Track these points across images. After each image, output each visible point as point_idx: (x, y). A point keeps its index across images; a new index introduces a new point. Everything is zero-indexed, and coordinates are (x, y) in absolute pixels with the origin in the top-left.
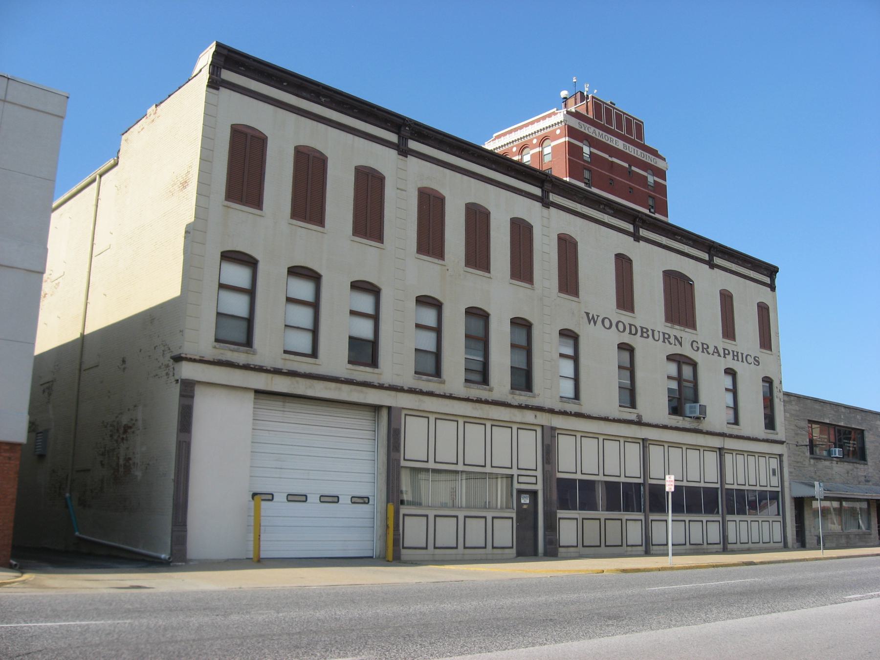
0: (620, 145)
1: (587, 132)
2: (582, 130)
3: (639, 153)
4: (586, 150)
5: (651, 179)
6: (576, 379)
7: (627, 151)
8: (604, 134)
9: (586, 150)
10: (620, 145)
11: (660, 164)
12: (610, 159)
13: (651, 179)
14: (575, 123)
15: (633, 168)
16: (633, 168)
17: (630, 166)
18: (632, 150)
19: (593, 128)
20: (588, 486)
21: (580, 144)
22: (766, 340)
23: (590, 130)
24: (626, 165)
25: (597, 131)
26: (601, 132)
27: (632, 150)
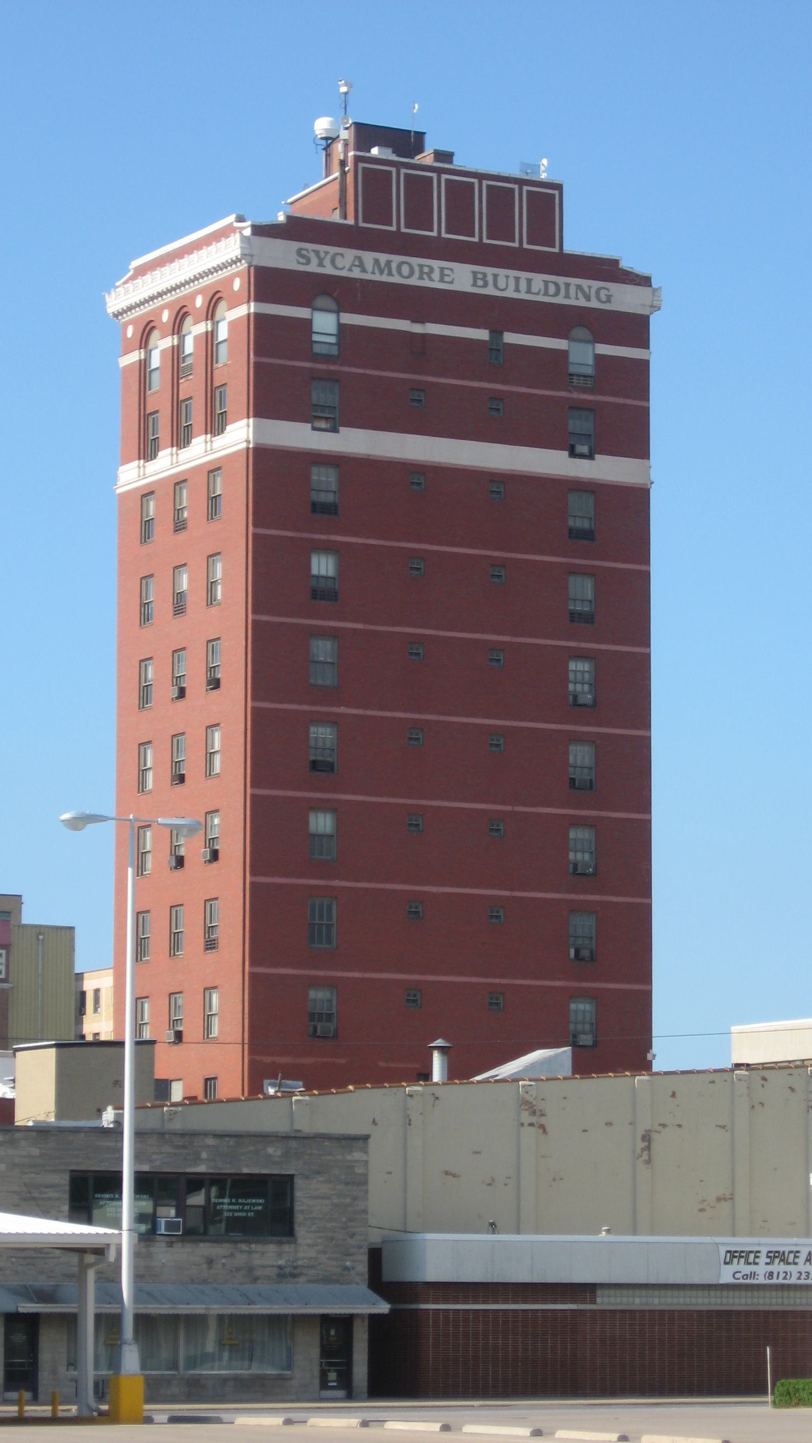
0: (461, 277)
1: (329, 270)
2: (313, 268)
3: (369, 265)
4: (325, 324)
5: (583, 354)
6: (7, 966)
7: (490, 291)
8: (396, 259)
9: (325, 324)
10: (461, 277)
11: (625, 299)
12: (417, 328)
13: (583, 354)
14: (284, 255)
15: (510, 338)
16: (510, 338)
17: (496, 333)
18: (535, 287)
19: (350, 254)
20: (320, 1015)
21: (301, 313)
22: (174, 1420)
23: (345, 263)
24: (482, 334)
25: (368, 257)
26: (383, 258)
27: (535, 287)
